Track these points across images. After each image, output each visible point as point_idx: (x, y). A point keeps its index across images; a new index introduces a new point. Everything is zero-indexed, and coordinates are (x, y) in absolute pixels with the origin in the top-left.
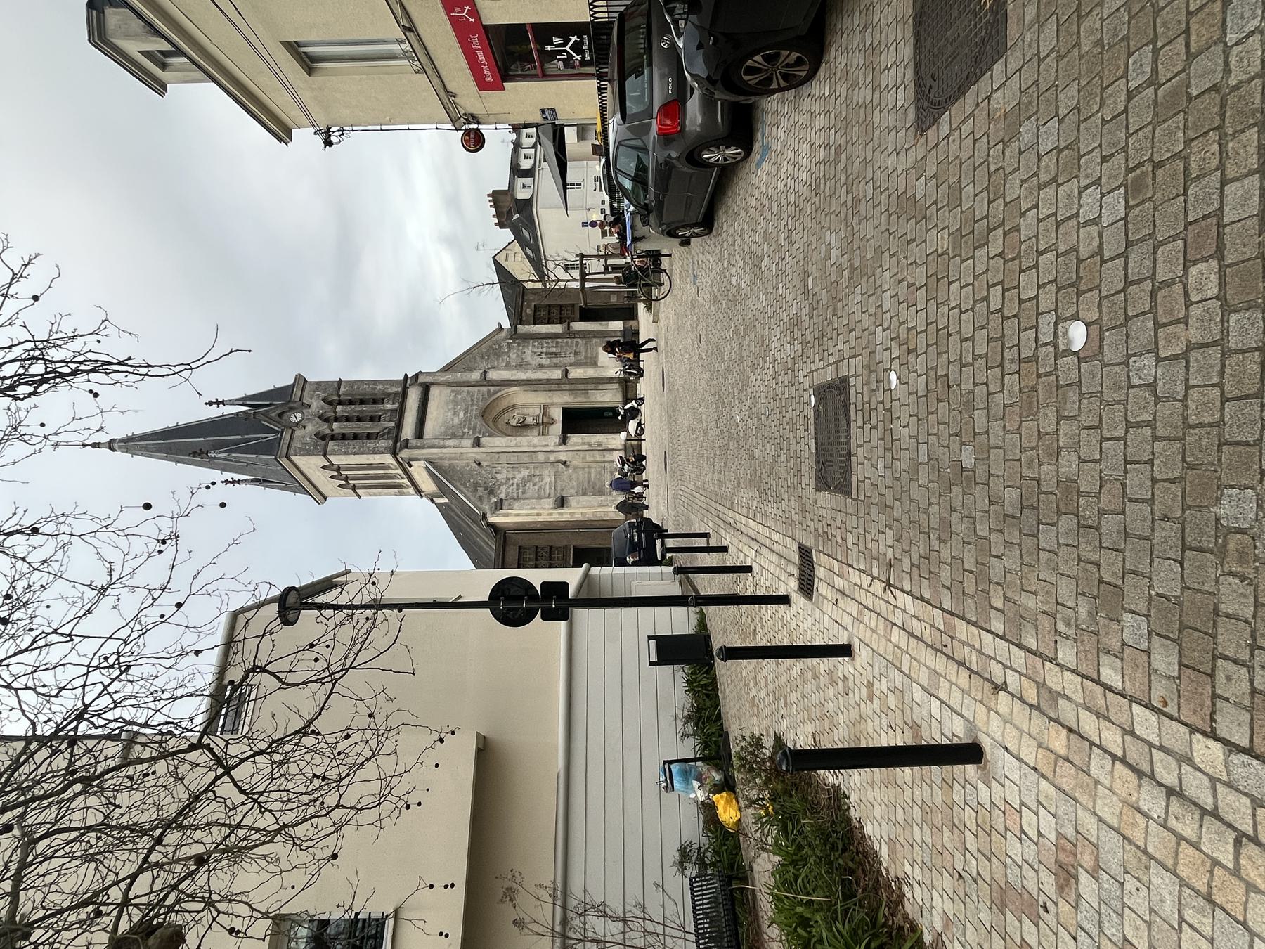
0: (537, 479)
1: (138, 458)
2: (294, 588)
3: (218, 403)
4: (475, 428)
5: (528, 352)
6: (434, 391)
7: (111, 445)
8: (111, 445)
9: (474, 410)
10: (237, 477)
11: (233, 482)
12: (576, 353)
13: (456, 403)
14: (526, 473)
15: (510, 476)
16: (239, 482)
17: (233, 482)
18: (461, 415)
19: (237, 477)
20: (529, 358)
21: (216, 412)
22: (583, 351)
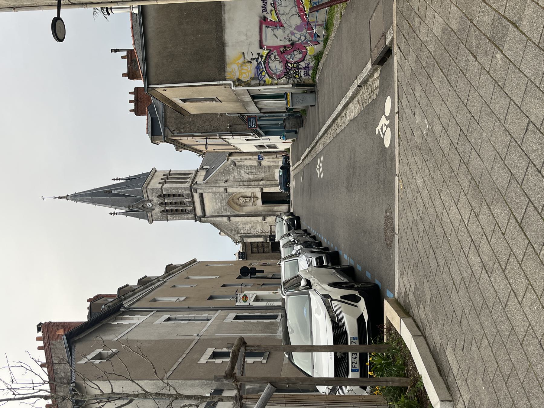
0: (254, 228)
1: (79, 203)
2: (141, 103)
3: (117, 179)
4: (226, 210)
5: (242, 172)
7: (67, 197)
8: (67, 197)
9: (224, 202)
11: (114, 213)
12: (265, 172)
13: (216, 199)
14: (250, 225)
15: (244, 226)
16: (117, 214)
17: (114, 213)
18: (219, 204)
19: (117, 211)
20: (243, 175)
21: (115, 182)
22: (268, 171)
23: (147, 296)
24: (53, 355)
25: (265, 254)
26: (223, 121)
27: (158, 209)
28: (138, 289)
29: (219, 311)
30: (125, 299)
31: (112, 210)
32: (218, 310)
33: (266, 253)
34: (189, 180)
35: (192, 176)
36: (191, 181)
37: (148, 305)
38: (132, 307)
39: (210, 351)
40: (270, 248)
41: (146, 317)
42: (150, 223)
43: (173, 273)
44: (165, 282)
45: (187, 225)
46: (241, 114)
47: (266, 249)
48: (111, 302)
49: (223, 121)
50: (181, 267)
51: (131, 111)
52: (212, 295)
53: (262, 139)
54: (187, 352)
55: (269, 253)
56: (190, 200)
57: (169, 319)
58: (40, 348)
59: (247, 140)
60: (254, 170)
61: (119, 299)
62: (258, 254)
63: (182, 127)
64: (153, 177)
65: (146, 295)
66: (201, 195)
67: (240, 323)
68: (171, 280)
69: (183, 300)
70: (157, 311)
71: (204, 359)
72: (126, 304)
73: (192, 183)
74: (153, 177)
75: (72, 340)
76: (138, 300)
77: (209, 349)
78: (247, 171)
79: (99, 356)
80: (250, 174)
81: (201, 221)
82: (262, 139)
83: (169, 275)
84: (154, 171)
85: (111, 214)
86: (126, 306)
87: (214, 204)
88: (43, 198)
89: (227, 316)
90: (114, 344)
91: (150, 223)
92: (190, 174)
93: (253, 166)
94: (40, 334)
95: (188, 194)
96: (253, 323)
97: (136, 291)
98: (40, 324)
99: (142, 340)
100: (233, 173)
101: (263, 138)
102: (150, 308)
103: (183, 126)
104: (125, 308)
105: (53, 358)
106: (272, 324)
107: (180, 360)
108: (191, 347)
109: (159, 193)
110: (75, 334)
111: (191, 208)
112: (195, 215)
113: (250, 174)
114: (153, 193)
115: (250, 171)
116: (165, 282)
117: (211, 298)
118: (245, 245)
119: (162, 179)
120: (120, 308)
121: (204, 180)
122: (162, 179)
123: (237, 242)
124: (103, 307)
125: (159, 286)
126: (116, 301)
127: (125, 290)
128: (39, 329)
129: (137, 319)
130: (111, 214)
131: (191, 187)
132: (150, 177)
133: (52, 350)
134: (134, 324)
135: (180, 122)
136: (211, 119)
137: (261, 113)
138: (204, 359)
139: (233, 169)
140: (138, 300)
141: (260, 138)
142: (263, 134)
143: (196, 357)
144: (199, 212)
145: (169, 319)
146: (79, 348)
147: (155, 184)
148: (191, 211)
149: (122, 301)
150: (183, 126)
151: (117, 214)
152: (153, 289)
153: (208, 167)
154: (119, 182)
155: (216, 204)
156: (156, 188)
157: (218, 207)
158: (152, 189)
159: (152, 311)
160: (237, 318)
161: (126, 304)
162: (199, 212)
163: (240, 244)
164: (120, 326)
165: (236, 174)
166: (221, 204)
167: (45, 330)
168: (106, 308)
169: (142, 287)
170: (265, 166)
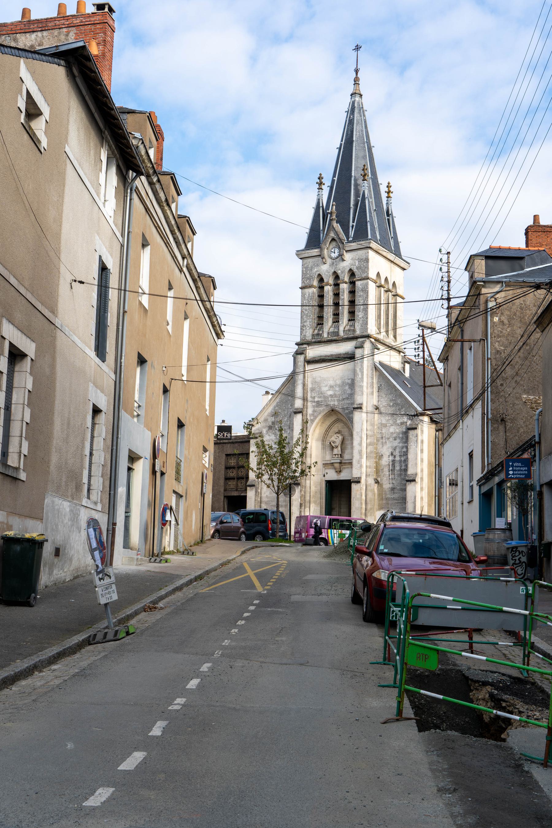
11: (321, 184)
18: (331, 393)
23: (93, 512)
24: (45, 33)
25: (222, 482)
26: (514, 404)
27: (325, 269)
28: (168, 212)
29: (113, 377)
30: (151, 184)
31: (327, 182)
32: (115, 373)
33: (226, 484)
34: (384, 334)
35: (390, 340)
36: (381, 337)
37: (137, 231)
38: (135, 196)
39: (28, 347)
40: (235, 494)
41: (111, 221)
42: (298, 253)
43: (197, 288)
44: (181, 270)
45: (290, 325)
46: (539, 443)
47: (232, 484)
48: (147, 153)
49: (514, 404)
50: (209, 306)
51: (536, 218)
52: (149, 363)
53: (472, 487)
54: (29, 296)
55: (225, 490)
56: (341, 333)
57: (96, 411)
58: (61, 7)
59: (471, 455)
60: (397, 468)
61: (151, 171)
62: (223, 467)
63: (503, 318)
64: (392, 262)
65: (157, 227)
66: (350, 357)
67: (85, 418)
68: (184, 285)
69: (140, 303)
70: (122, 246)
71: (11, 333)
72: (141, 183)
73: (377, 340)
74: (392, 262)
75: (71, 60)
76: (147, 209)
77: (33, 346)
78: (397, 453)
79: (33, 112)
80: (391, 458)
81: (297, 353)
82: (472, 487)
83: (194, 281)
84: (403, 264)
85: (320, 178)
86: (137, 182)
87: (331, 383)
88: (357, 48)
89: (102, 391)
90: (59, 138)
91: (298, 253)
92: (395, 337)
93: (407, 466)
94: (90, 9)
95: (354, 331)
96: (83, 447)
97: (166, 208)
98: (111, 10)
99: (62, 205)
100: (395, 423)
101: (476, 489)
102: (129, 232)
103: (506, 322)
104: (134, 179)
105: (39, 34)
106: (78, 487)
107: (13, 280)
108: (40, 307)
109: (357, 273)
110: (84, 71)
111: (325, 335)
112: (309, 344)
113: (391, 458)
114: (360, 260)
115: (398, 458)
116: (181, 270)
117: (142, 361)
118: (245, 441)
119: (386, 279)
120: (134, 171)
121: (381, 363)
122: (386, 279)
123: (249, 426)
124: (138, 135)
125: (174, 257)
126: (149, 165)
127: (169, 187)
128: (100, 7)
129: (110, 206)
130: (320, 178)
131: (368, 337)
132: (391, 256)
133: (56, 32)
134: (98, 194)
135: (515, 314)
136: (518, 379)
137: (541, 486)
138: (11, 333)
139: (402, 423)
140: (147, 209)
141: (475, 483)
142: (485, 489)
143: (18, 316)
144: (312, 352)
145: (103, 269)
146: (58, 72)
147: (378, 264)
148: (318, 334)
149: (148, 176)
150: (506, 322)
151: (320, 188)
152: (167, 244)
153: (407, 374)
154: (384, 196)
155: (331, 387)
156: (367, 268)
157: (324, 389)
158: (367, 260)
159: (123, 235)
160: (96, 411)
161: (141, 183)
162: (312, 352)
163: (245, 433)
164: (96, 165)
165: (392, 430)
166: (331, 396)
167: (98, 18)
168: (134, 142)
169: (173, 222)
170: (405, 490)
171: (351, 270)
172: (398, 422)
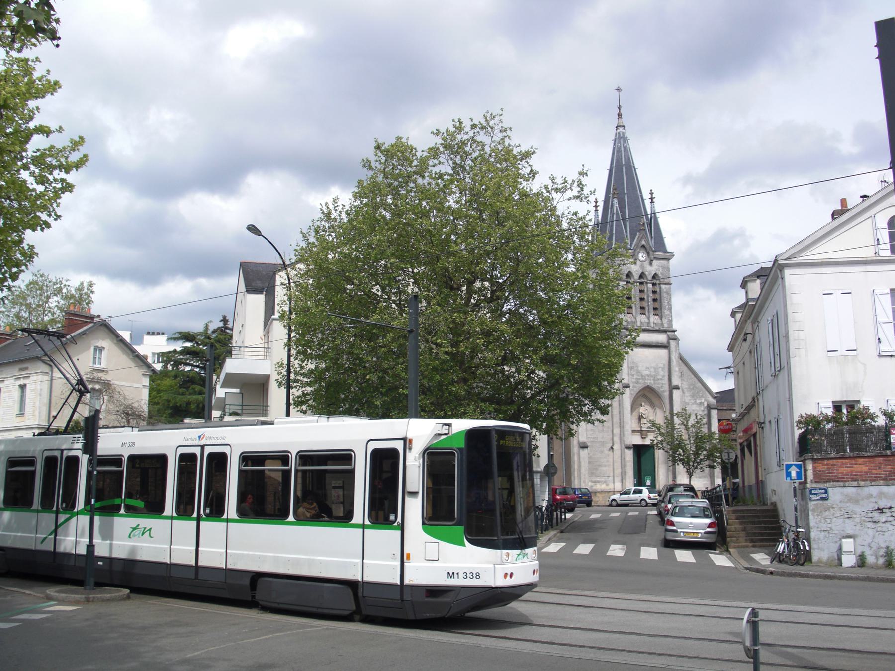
6: (663, 352)
10: (600, 209)
18: (647, 373)
21: (646, 196)
100: (695, 403)
157: (640, 369)
166: (648, 376)
171: (655, 274)
172: (698, 401)
